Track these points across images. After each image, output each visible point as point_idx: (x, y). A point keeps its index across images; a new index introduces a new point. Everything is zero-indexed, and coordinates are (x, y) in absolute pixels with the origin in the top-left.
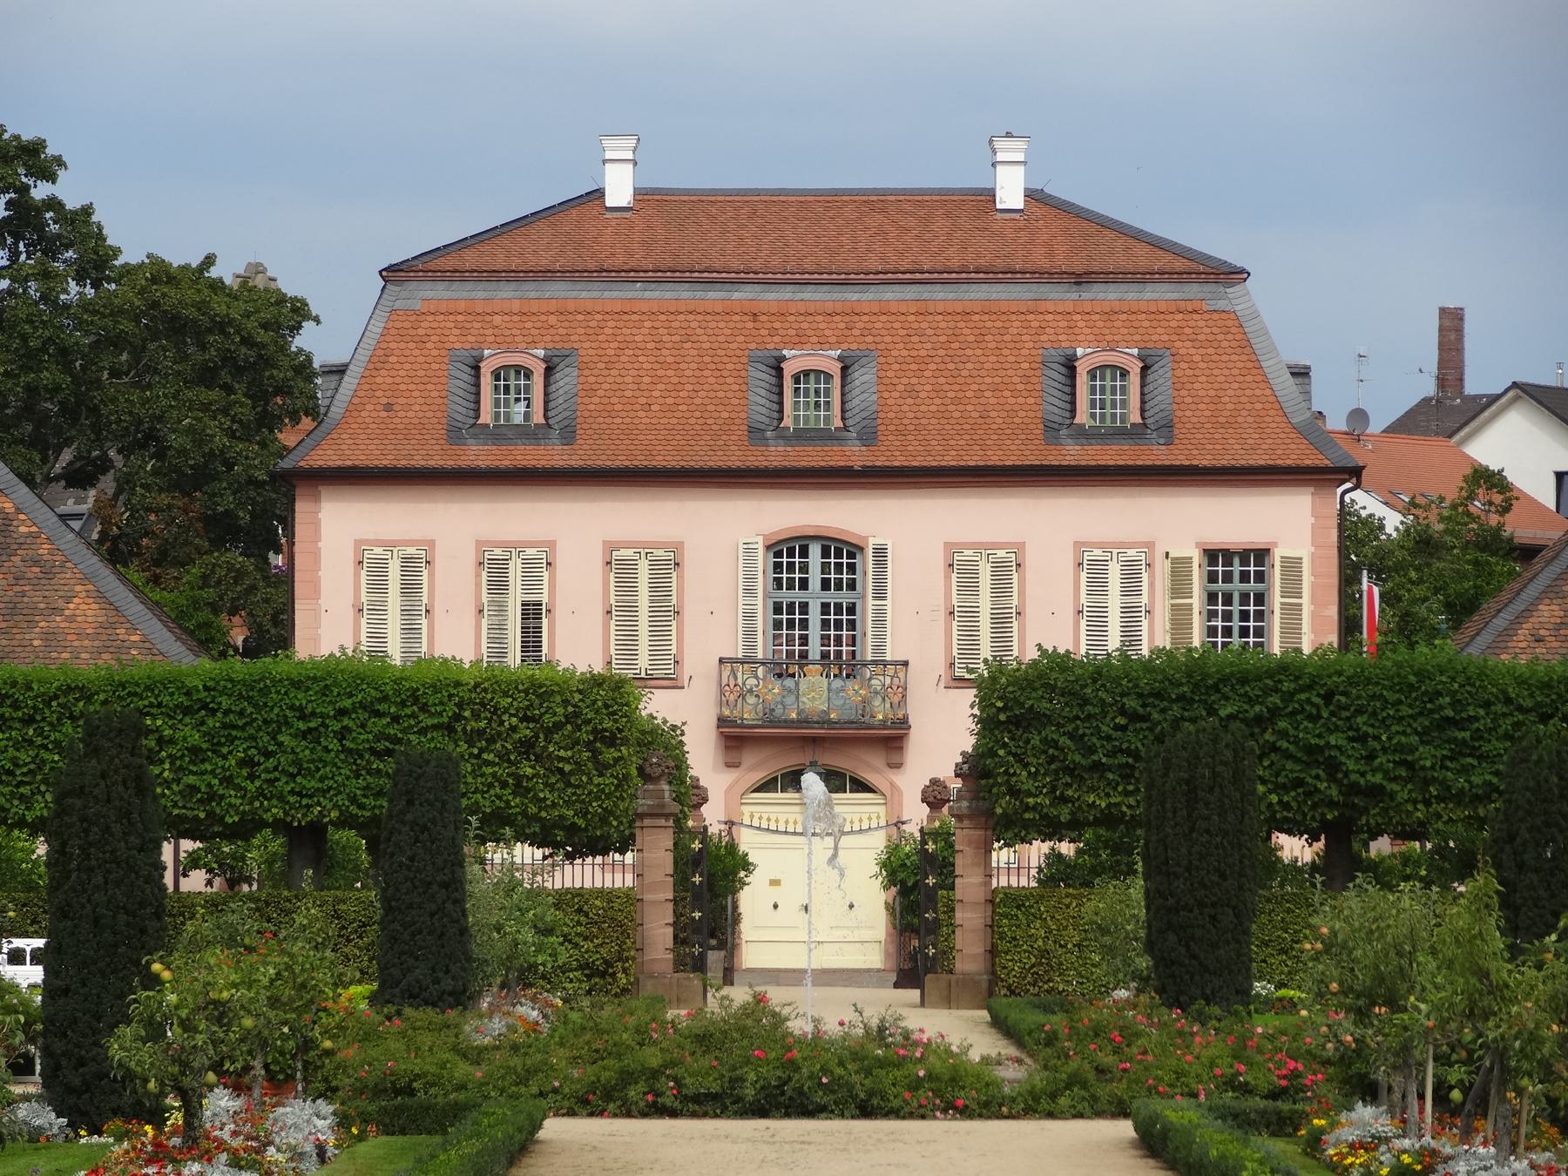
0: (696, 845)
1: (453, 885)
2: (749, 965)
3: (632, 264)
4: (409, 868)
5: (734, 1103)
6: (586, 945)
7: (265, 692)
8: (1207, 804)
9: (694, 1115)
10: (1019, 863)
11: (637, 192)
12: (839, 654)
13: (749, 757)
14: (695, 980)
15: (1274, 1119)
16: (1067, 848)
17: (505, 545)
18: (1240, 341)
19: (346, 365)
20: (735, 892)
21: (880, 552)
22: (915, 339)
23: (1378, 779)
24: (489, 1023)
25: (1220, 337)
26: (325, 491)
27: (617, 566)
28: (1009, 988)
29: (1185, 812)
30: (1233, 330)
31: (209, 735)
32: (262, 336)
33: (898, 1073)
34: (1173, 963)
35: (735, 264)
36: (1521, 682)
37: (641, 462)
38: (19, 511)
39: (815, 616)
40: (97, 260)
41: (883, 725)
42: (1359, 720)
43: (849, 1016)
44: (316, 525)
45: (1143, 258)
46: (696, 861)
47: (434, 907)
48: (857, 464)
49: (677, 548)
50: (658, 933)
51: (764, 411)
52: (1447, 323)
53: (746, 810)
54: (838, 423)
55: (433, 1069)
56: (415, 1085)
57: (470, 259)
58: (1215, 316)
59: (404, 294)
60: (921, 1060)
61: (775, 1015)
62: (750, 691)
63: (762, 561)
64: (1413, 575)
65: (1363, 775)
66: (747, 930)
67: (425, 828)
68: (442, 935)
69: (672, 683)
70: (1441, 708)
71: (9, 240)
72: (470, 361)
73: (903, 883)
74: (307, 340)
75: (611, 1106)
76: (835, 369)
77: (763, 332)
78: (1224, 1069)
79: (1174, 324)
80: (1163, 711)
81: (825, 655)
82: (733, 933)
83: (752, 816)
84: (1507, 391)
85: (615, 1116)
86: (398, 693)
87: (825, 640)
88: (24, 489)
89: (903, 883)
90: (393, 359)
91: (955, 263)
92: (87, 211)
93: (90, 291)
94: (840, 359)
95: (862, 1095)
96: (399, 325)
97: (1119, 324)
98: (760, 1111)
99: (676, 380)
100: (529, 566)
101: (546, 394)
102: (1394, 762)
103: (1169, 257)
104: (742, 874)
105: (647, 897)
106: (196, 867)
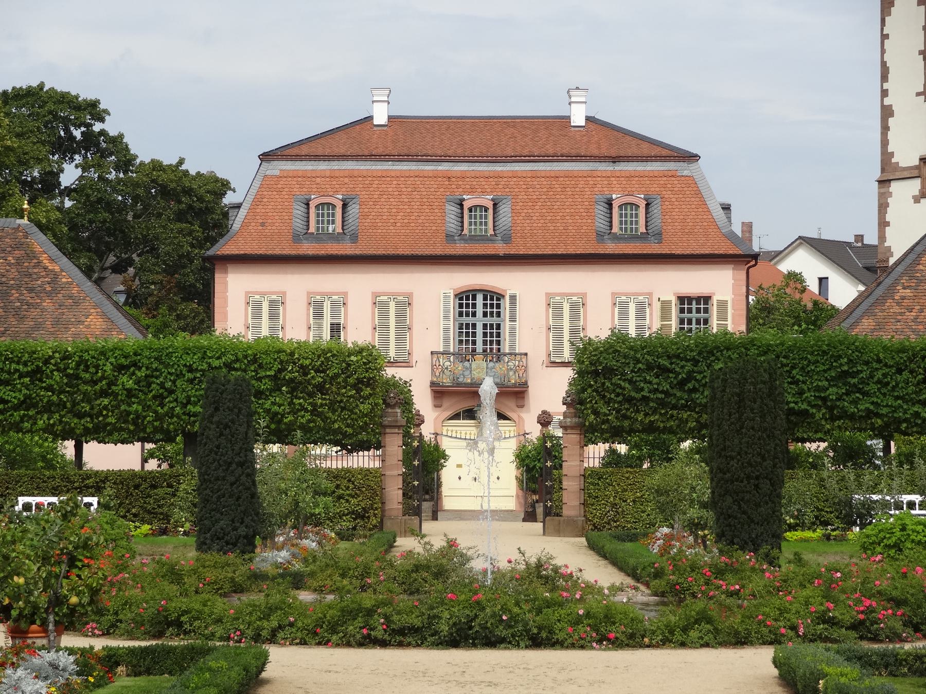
0: (416, 444)
1: (247, 462)
2: (446, 508)
3: (387, 152)
4: (216, 454)
5: (432, 635)
6: (353, 501)
7: (169, 355)
8: (752, 410)
9: (400, 645)
10: (596, 453)
11: (390, 118)
12: (491, 349)
13: (446, 403)
14: (415, 520)
15: (892, 660)
16: (622, 449)
17: (322, 294)
18: (694, 192)
19: (241, 204)
20: (438, 471)
21: (513, 298)
22: (531, 190)
23: (804, 406)
24: (274, 556)
25: (685, 189)
26: (230, 268)
27: (380, 306)
28: (594, 525)
29: (737, 415)
30: (693, 185)
31: (137, 382)
32: (209, 197)
33: (562, 612)
34: (729, 516)
35: (439, 152)
36: (885, 349)
37: (391, 252)
38: (62, 271)
39: (479, 330)
40: (126, 161)
41: (515, 386)
42: (794, 372)
43: (515, 556)
44: (226, 284)
45: (646, 149)
46: (416, 452)
47: (233, 479)
48: (501, 253)
49: (409, 296)
50: (394, 494)
51: (453, 226)
52: (745, 228)
53: (445, 428)
54: (491, 232)
55: (197, 606)
56: (182, 619)
57: (305, 150)
58: (683, 178)
59: (270, 167)
60: (581, 600)
61: (462, 555)
62: (447, 368)
63: (452, 303)
64: (761, 321)
65: (796, 403)
66: (445, 490)
67: (226, 426)
68: (238, 498)
69: (407, 364)
70: (841, 365)
71: (83, 152)
72: (305, 201)
73: (527, 465)
74: (229, 199)
75: (334, 637)
76: (490, 205)
77: (453, 186)
78: (817, 607)
79: (662, 182)
80: (683, 367)
81: (485, 351)
82: (438, 491)
83: (447, 430)
84: (796, 240)
85: (338, 645)
86: (246, 357)
87: (485, 343)
88: (65, 259)
89: (527, 465)
90: (265, 200)
91: (551, 152)
92: (121, 136)
93: (121, 175)
94: (492, 200)
95: (535, 631)
96: (268, 183)
97: (634, 182)
98: (453, 643)
99: (408, 211)
100: (334, 304)
101: (343, 218)
102: (815, 396)
103: (659, 149)
104: (443, 461)
105: (387, 473)
106: (153, 458)
